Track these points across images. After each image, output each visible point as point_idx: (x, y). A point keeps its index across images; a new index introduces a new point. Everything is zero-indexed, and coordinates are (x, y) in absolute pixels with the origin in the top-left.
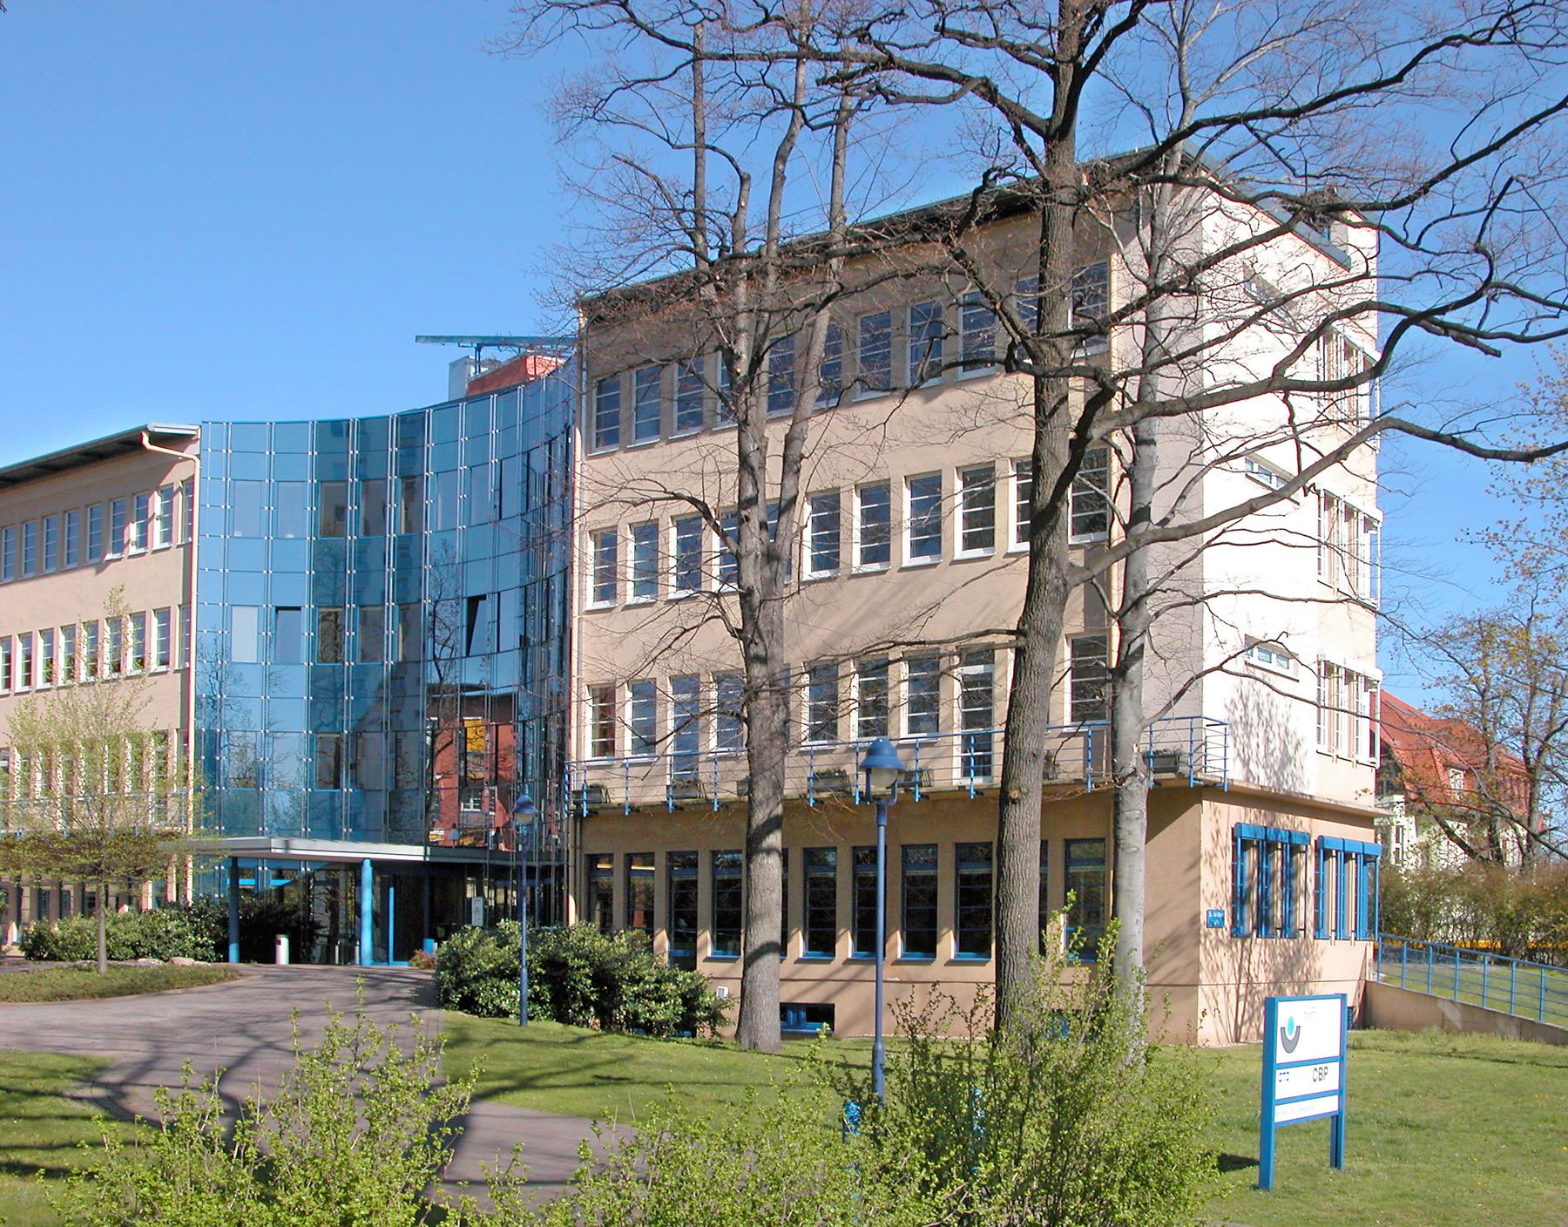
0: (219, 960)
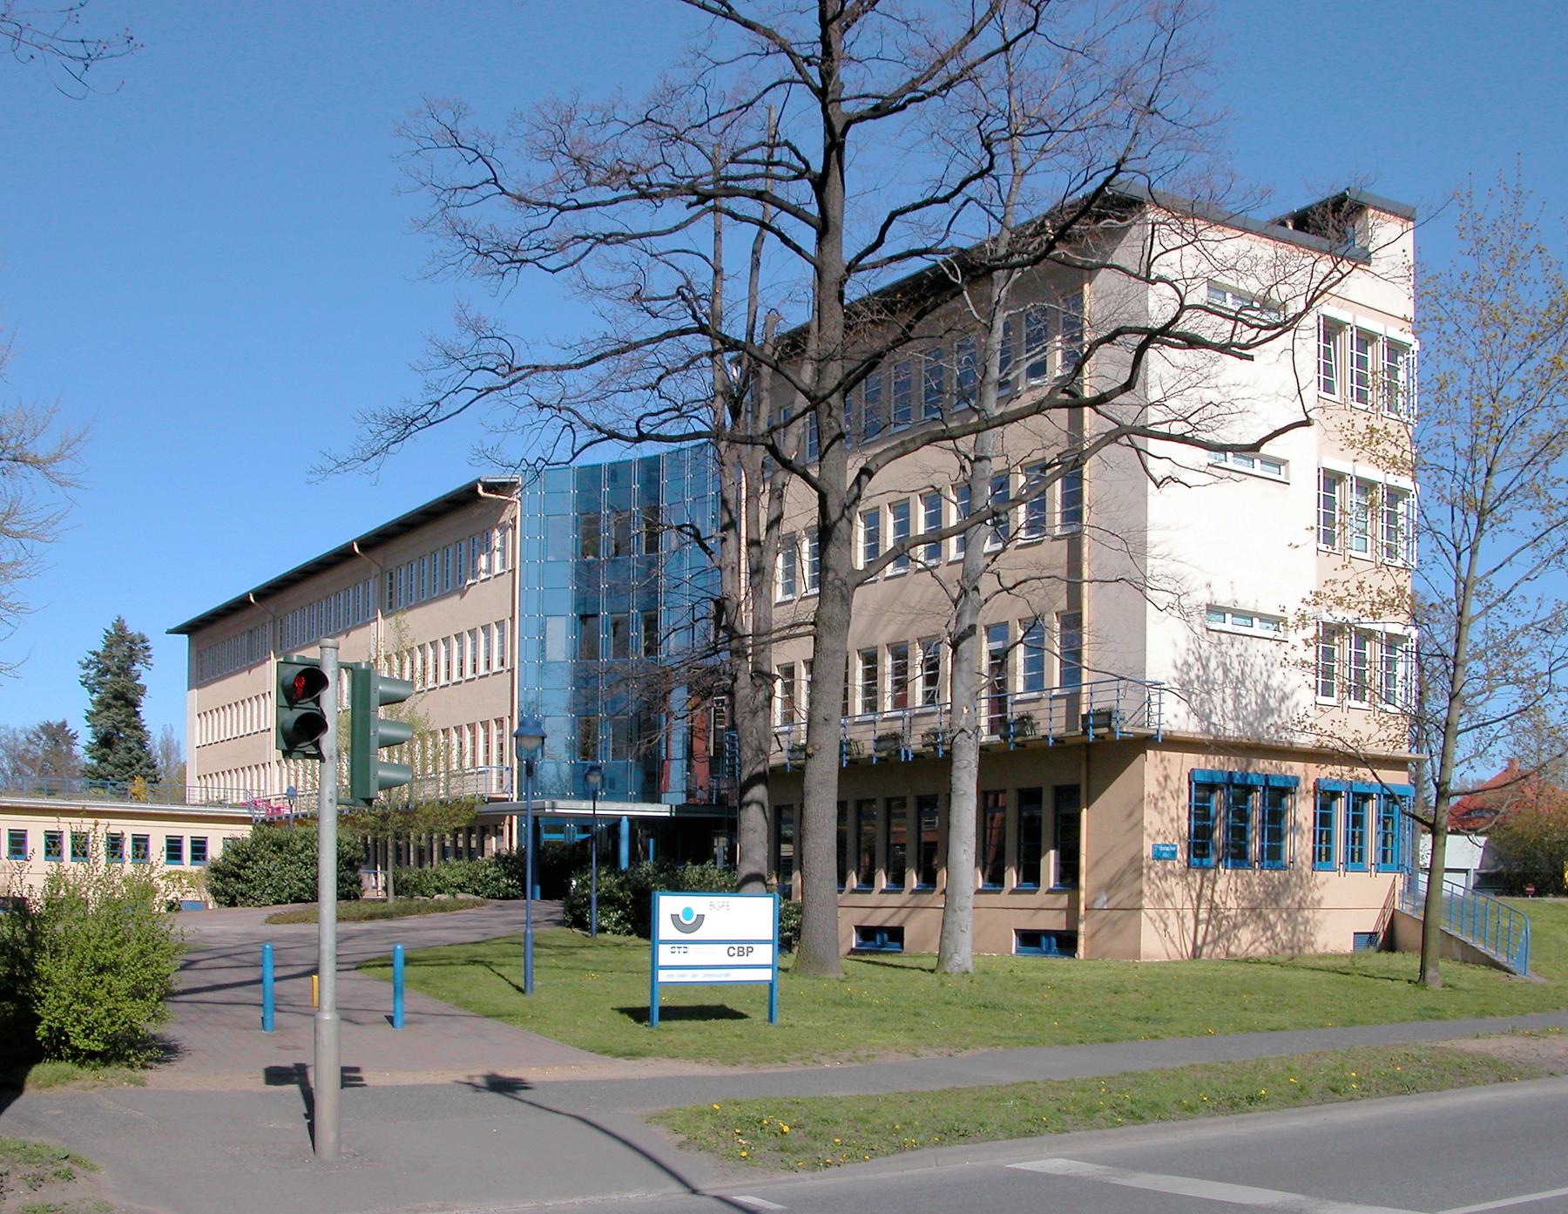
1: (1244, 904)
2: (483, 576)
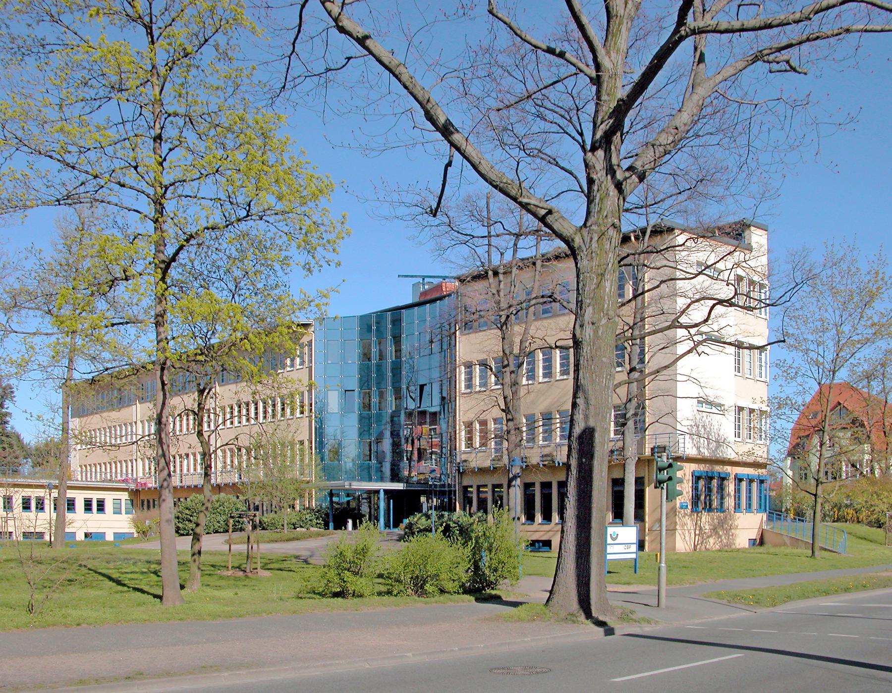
0: (325, 529)
1: (712, 527)
2: (289, 369)
